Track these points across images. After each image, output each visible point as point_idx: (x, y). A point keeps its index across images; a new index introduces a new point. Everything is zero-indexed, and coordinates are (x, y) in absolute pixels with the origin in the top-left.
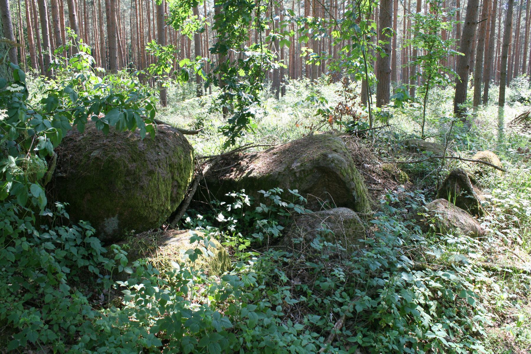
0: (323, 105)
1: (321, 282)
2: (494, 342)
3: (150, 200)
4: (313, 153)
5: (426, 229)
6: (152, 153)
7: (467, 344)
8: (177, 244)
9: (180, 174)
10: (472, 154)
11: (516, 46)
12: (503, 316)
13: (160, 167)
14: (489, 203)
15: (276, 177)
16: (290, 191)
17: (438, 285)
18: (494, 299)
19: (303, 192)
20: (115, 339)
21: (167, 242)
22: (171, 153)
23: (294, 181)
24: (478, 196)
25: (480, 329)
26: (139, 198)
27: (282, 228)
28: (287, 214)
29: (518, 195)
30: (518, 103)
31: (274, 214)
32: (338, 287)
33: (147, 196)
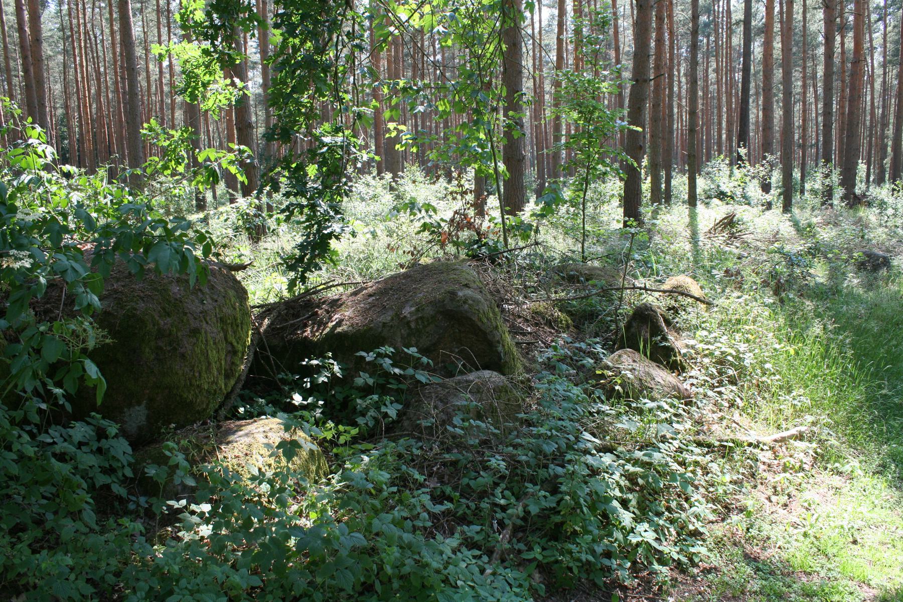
0: (430, 217)
1: (471, 479)
2: (719, 542)
3: (197, 374)
4: (426, 291)
5: (610, 394)
6: (193, 301)
7: (684, 548)
8: (247, 440)
9: (235, 332)
10: (660, 281)
11: (705, 112)
12: (726, 507)
13: (207, 323)
14: (693, 351)
15: (380, 330)
16: (406, 350)
17: (638, 469)
18: (712, 485)
19: (424, 351)
20: (189, 583)
21: (231, 438)
22: (220, 299)
23: (409, 335)
24: (676, 343)
25: (698, 525)
26: (180, 372)
27: (400, 407)
28: (401, 386)
29: (731, 337)
30: (716, 201)
31: (383, 385)
32: (496, 484)
33: (192, 370)
